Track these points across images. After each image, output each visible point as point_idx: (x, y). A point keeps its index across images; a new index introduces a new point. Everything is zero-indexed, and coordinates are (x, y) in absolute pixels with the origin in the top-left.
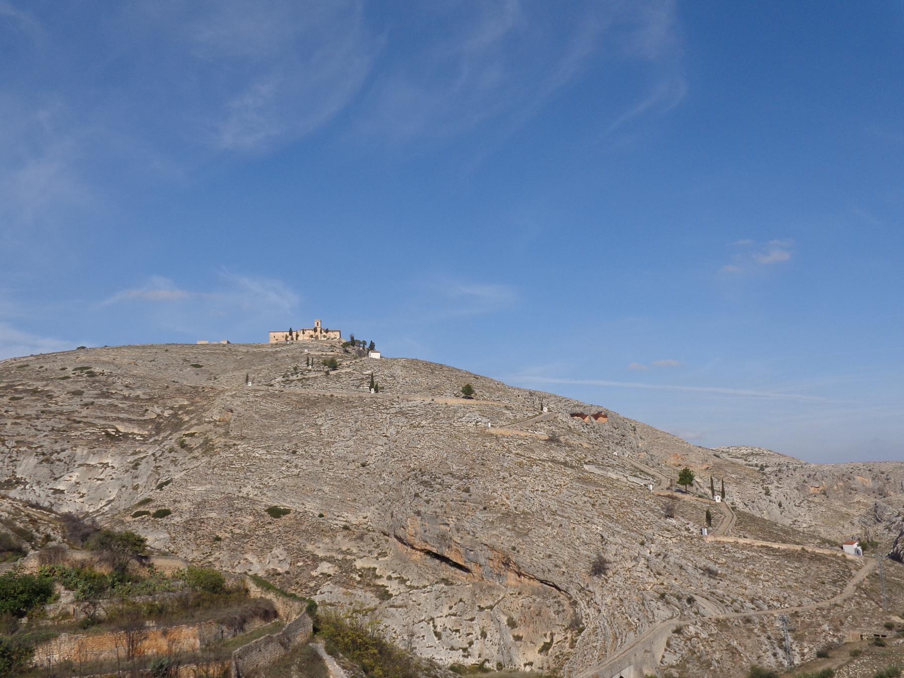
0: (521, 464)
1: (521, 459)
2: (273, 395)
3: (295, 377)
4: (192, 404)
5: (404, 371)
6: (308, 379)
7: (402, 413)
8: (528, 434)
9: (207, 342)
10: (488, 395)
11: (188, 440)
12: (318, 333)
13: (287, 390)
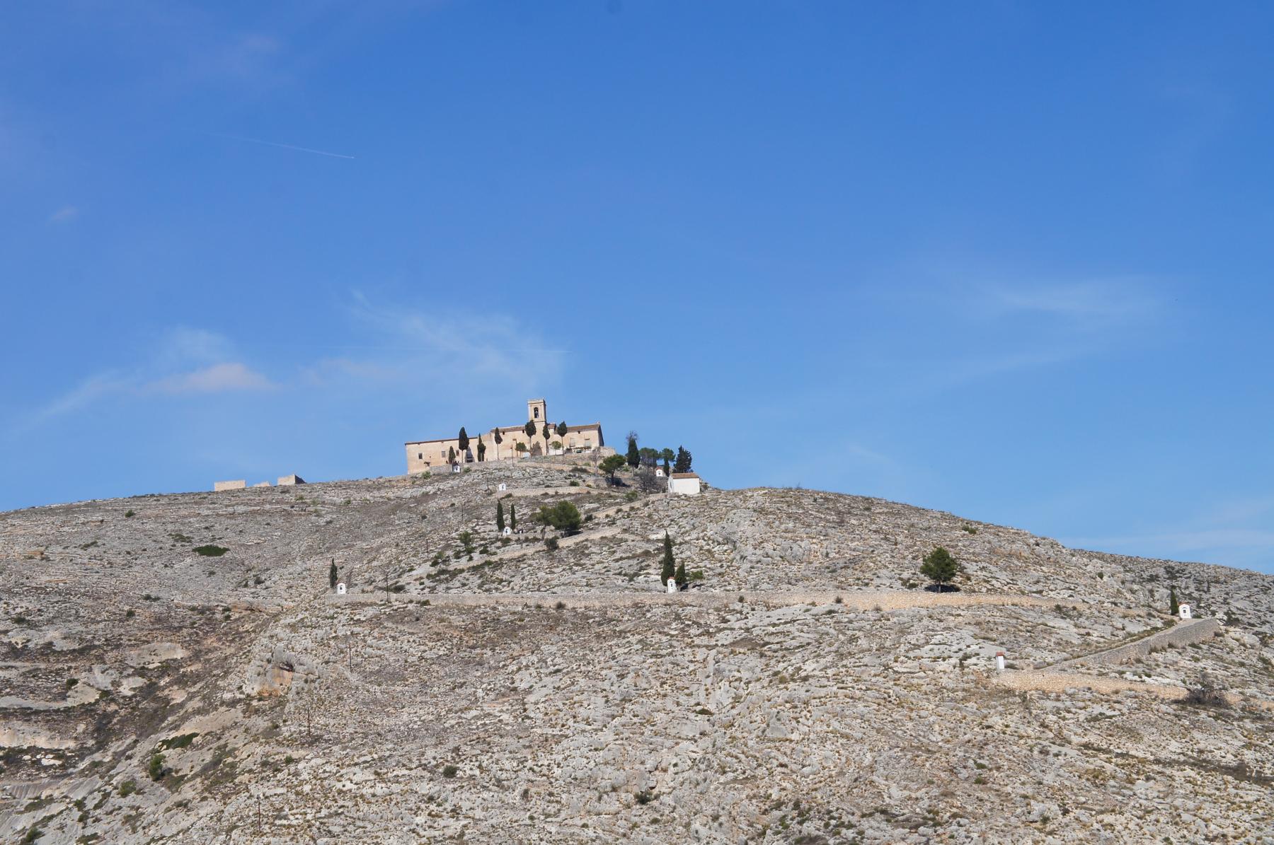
0: (1097, 777)
1: (1098, 761)
2: (399, 617)
3: (463, 563)
4: (196, 656)
5: (761, 524)
6: (498, 565)
7: (751, 643)
8: (1122, 685)
9: (240, 485)
10: (1004, 576)
11: (172, 757)
12: (538, 437)
13: (442, 597)
